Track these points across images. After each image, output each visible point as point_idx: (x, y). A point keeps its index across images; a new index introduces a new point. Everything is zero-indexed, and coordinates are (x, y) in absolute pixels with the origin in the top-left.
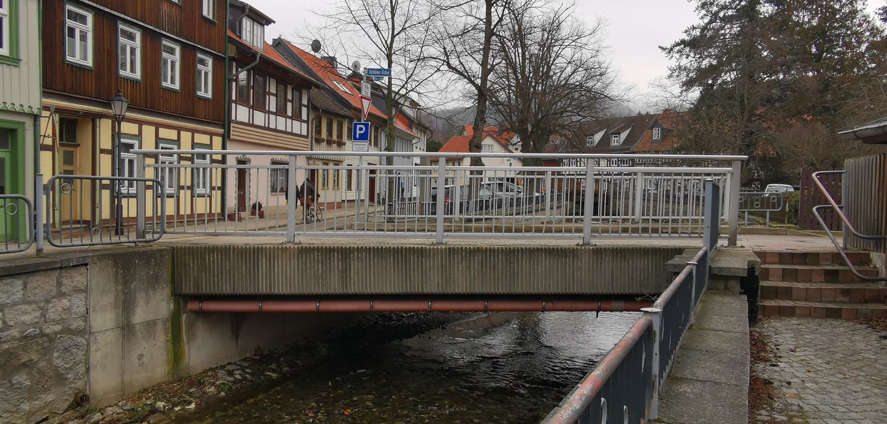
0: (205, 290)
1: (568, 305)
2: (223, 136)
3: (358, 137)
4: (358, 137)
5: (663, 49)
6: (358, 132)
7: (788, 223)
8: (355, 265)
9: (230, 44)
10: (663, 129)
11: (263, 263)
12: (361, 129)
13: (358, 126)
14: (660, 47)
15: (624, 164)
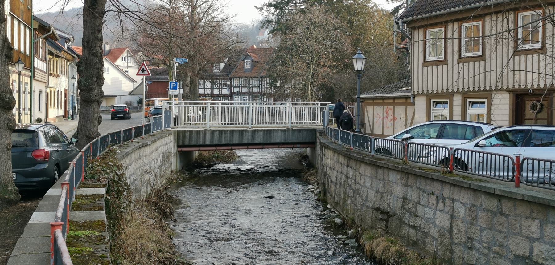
0: (186, 143)
1: (285, 146)
2: (31, 77)
3: (172, 88)
4: (172, 88)
5: (257, 8)
6: (172, 86)
7: (531, 44)
8: (228, 135)
9: (34, 21)
10: (252, 61)
11: (202, 135)
12: (174, 85)
13: (172, 83)
14: (255, 7)
15: (224, 86)
